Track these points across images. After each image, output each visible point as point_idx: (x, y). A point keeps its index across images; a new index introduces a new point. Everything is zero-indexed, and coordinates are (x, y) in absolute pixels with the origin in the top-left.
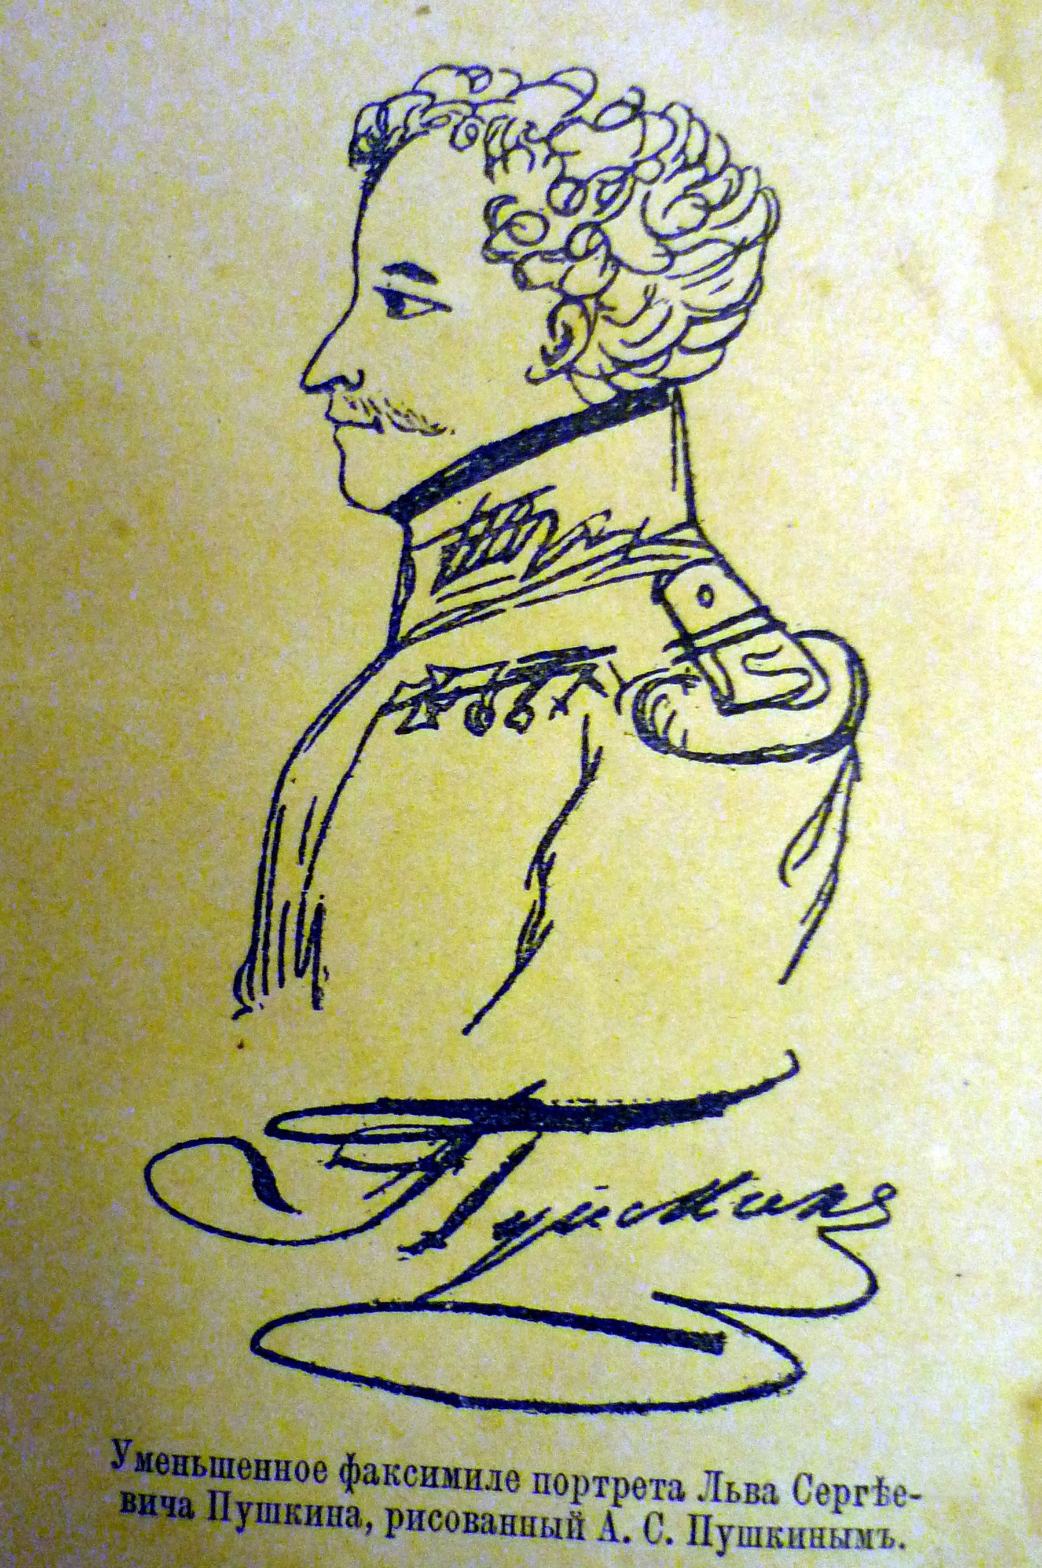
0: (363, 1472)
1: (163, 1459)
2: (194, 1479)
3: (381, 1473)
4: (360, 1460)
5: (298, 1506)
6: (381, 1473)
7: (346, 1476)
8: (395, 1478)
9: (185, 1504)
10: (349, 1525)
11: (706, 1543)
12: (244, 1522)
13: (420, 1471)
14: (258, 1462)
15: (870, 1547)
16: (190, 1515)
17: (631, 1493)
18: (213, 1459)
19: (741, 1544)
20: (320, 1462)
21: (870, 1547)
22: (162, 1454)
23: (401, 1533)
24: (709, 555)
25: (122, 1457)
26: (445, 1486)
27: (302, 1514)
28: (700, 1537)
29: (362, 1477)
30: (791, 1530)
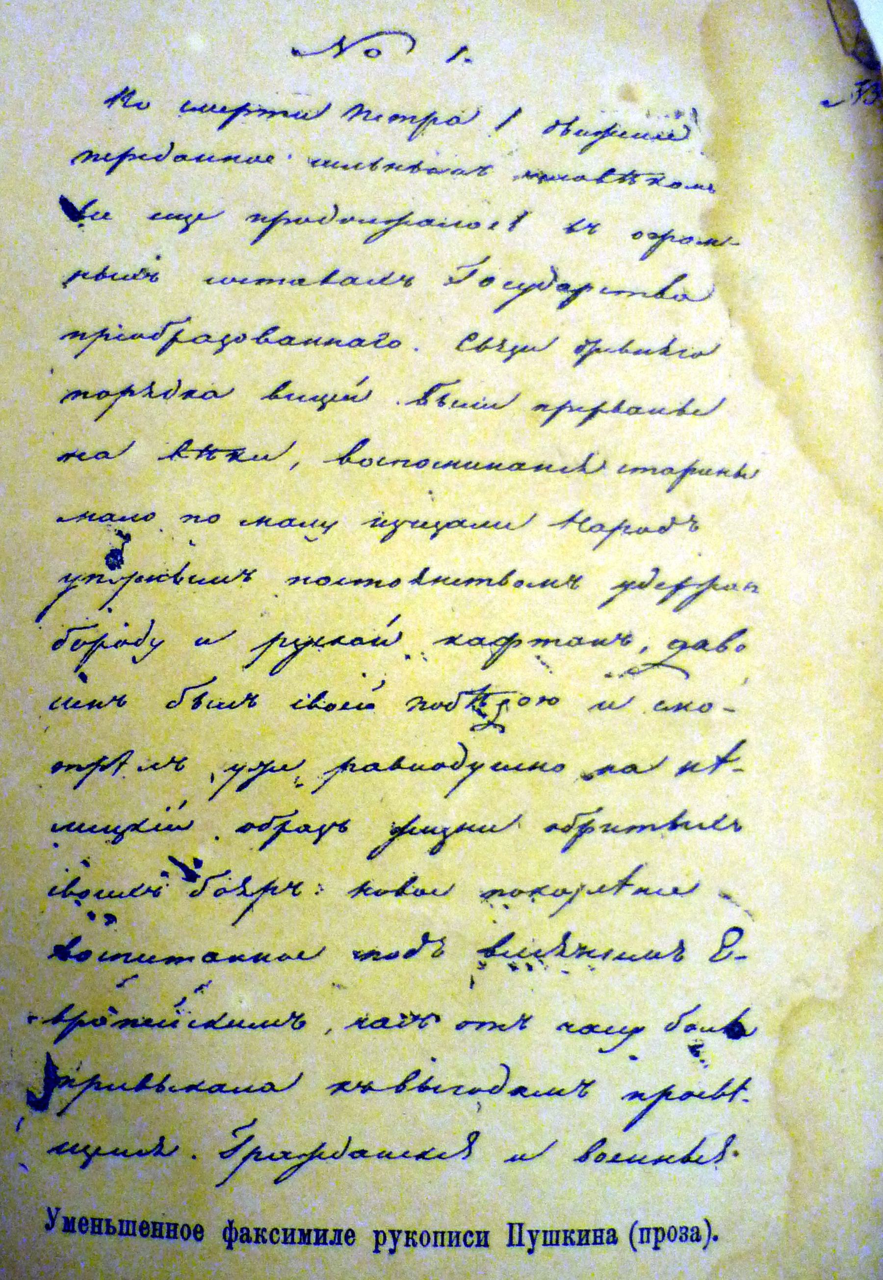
0: (240, 1234)
1: (83, 1222)
2: (107, 1237)
3: (253, 1235)
4: (238, 1226)
5: (573, 1232)
6: (253, 1235)
7: (228, 1236)
11: (520, 1244)
13: (475, 1236)
17: (192, 1237)
18: (121, 1222)
20: (672, 1241)
22: (350, 1230)
24: (89, 647)
25: (53, 1220)
26: (300, 1243)
28: (516, 1240)
29: (678, 1236)
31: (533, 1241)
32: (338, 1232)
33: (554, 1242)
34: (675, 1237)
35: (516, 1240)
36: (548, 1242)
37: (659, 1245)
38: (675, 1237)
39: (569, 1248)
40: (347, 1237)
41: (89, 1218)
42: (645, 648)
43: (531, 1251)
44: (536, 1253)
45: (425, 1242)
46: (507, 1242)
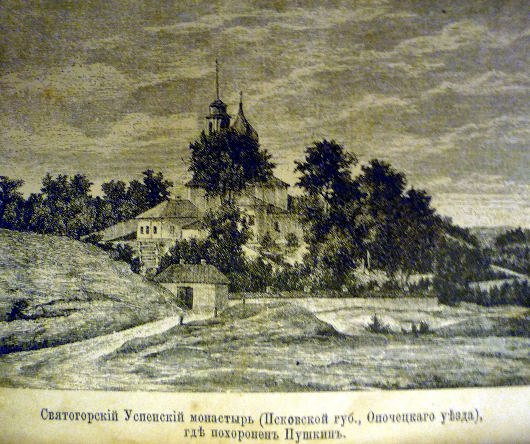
25: (129, 416)
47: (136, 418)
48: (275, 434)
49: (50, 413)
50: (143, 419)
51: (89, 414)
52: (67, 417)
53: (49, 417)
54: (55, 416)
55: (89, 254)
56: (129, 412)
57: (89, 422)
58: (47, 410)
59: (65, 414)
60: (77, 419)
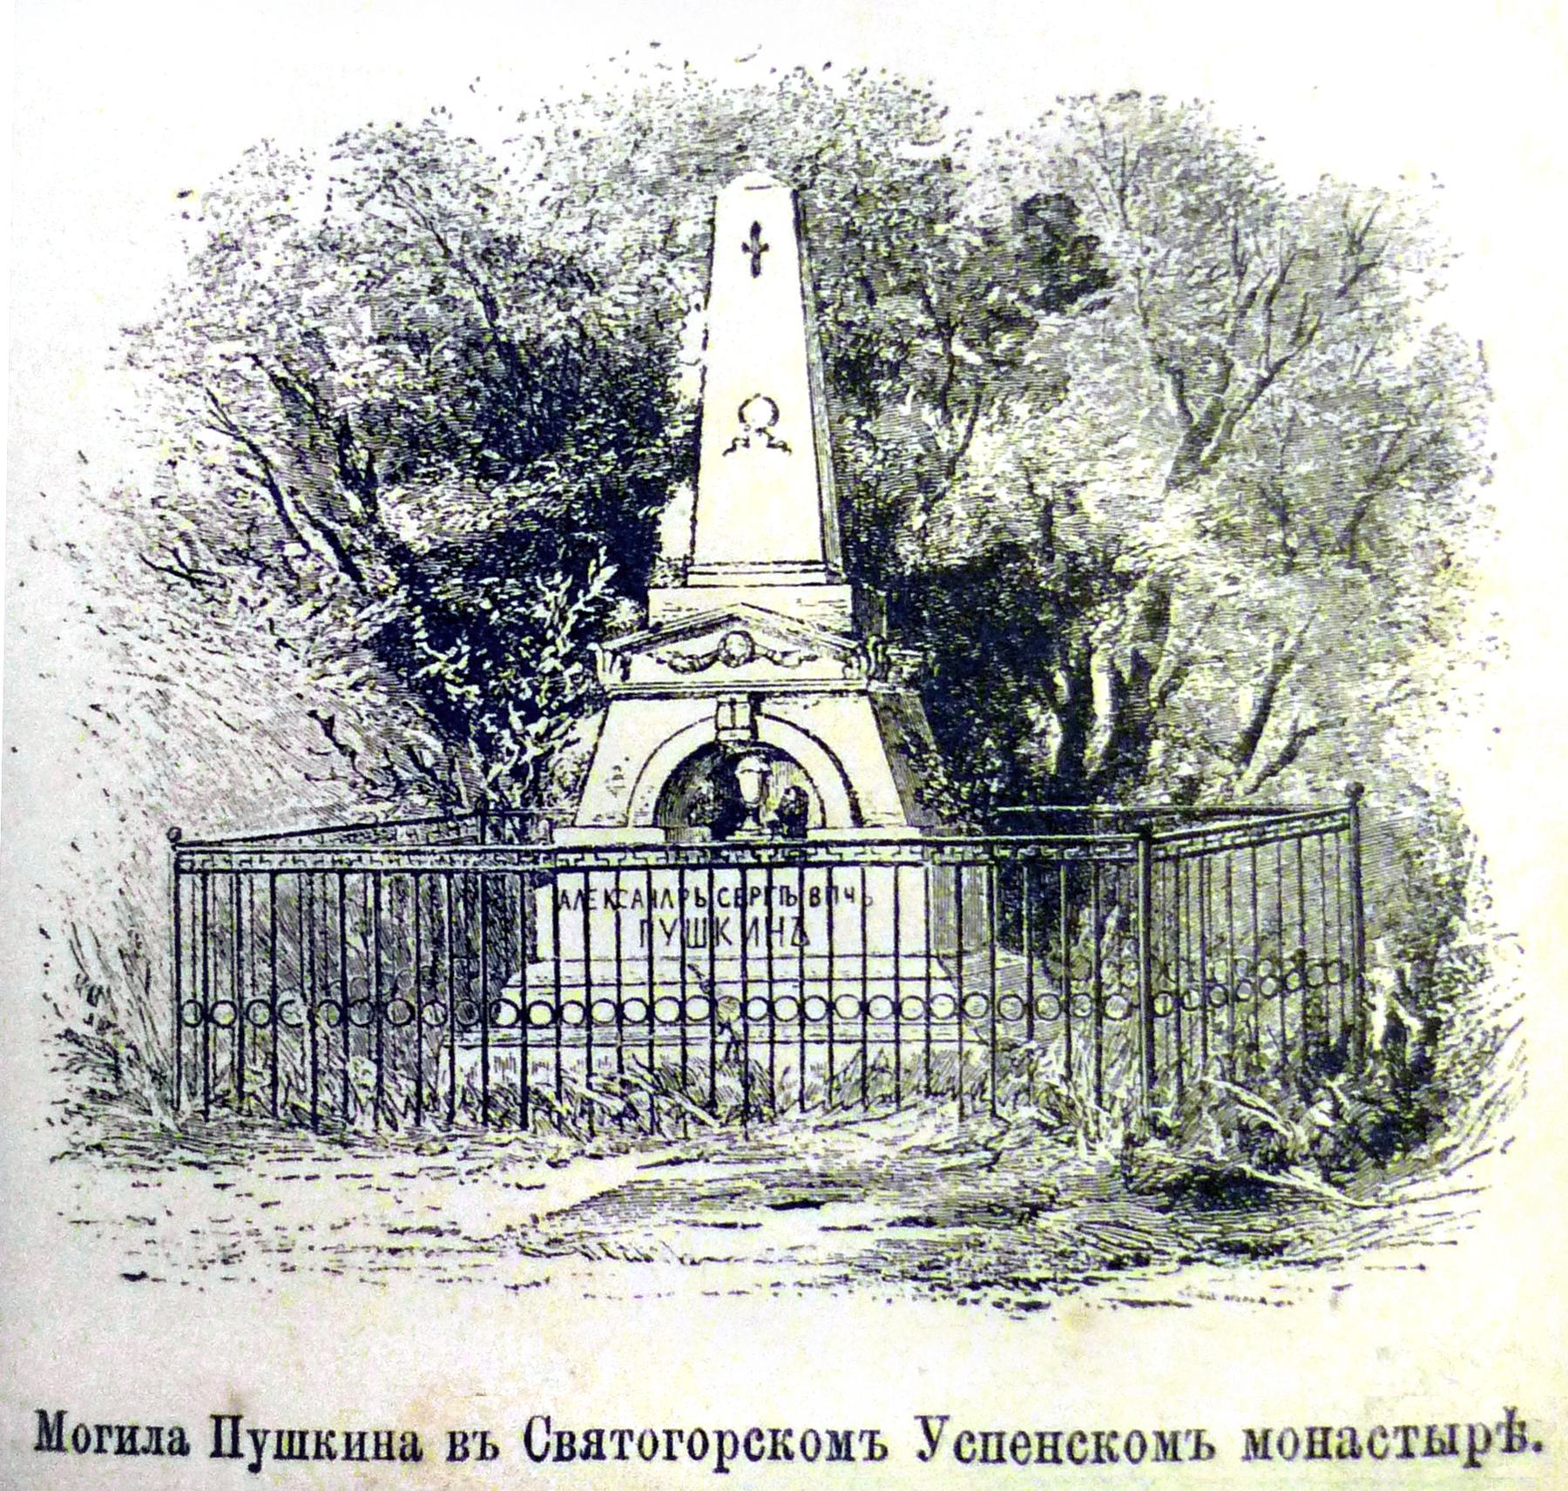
8: (786, 1449)
9: (177, 1434)
10: (403, 1457)
11: (236, 1454)
12: (259, 1456)
14: (1041, 1436)
15: (849, 1458)
16: (184, 1450)
19: (279, 1456)
21: (849, 1458)
23: (739, 1464)
25: (934, 1444)
27: (338, 1444)
28: (227, 1446)
30: (348, 1436)
31: (259, 1449)
32: (156, 1432)
33: (296, 1451)
34: (818, 1450)
35: (227, 1446)
36: (285, 1452)
37: (1478, 1458)
38: (818, 1450)
39: (324, 1464)
40: (1014, 1447)
41: (1030, 1433)
42: (42, 931)
43: (255, 1468)
44: (264, 1474)
45: (1135, 1452)
46: (212, 1448)
47: (966, 1451)
48: (1198, 1438)
49: (560, 1435)
50: (992, 1454)
51: (721, 1435)
52: (631, 1448)
53: (553, 1452)
54: (580, 1444)
55: (896, 83)
56: (934, 1426)
57: (721, 1469)
58: (548, 1421)
59: (622, 1436)
60: (670, 1456)
